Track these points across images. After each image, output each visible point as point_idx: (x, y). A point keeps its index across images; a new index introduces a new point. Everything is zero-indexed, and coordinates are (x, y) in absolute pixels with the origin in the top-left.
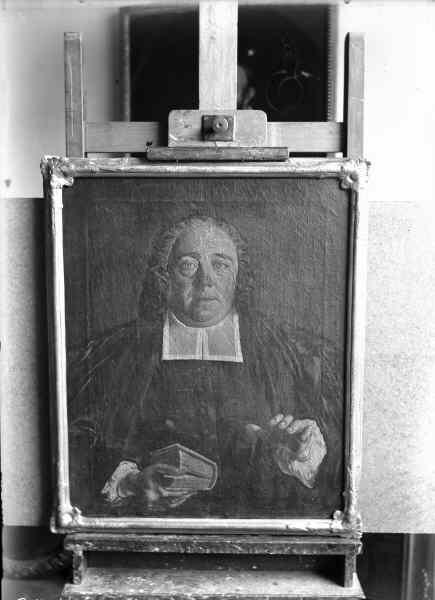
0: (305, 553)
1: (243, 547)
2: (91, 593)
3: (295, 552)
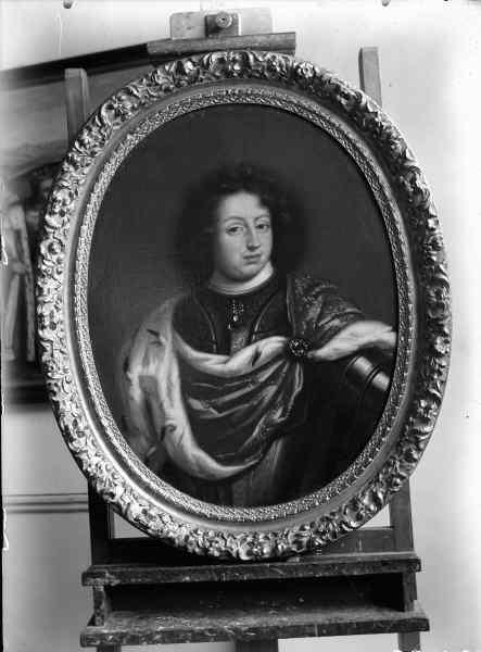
0: (355, 573)
1: (285, 571)
2: (114, 631)
3: (344, 572)
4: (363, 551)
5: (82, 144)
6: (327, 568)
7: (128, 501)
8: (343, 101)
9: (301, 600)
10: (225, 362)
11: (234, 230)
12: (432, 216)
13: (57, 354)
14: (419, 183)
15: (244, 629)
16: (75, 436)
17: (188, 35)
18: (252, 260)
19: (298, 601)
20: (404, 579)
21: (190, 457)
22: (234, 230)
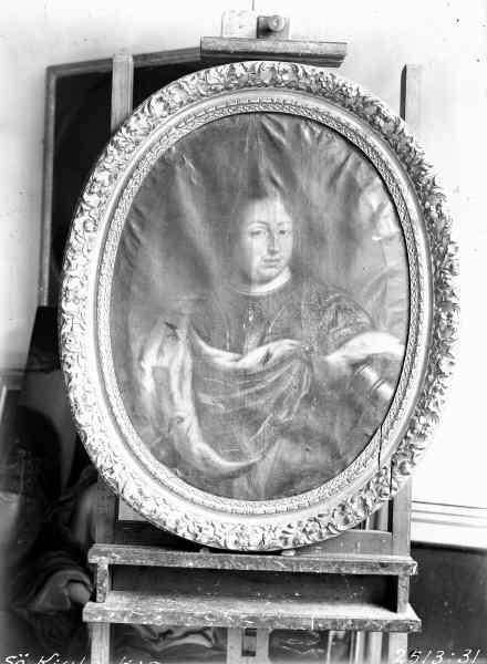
1: (287, 565)
4: (361, 553)
5: (129, 130)
6: (328, 565)
7: (125, 478)
8: (382, 123)
9: (199, 589)
10: (237, 360)
11: (258, 233)
12: (452, 243)
13: (77, 329)
14: (443, 209)
15: (243, 616)
16: (83, 410)
17: (239, 34)
18: (273, 264)
19: (197, 591)
20: (400, 581)
21: (195, 451)
22: (258, 233)
